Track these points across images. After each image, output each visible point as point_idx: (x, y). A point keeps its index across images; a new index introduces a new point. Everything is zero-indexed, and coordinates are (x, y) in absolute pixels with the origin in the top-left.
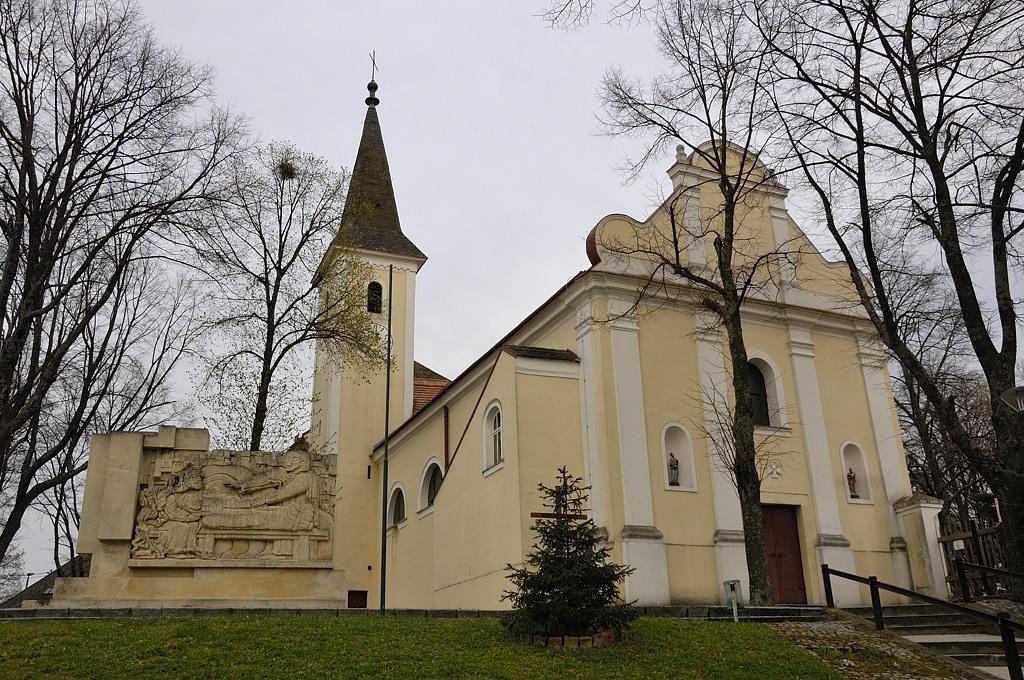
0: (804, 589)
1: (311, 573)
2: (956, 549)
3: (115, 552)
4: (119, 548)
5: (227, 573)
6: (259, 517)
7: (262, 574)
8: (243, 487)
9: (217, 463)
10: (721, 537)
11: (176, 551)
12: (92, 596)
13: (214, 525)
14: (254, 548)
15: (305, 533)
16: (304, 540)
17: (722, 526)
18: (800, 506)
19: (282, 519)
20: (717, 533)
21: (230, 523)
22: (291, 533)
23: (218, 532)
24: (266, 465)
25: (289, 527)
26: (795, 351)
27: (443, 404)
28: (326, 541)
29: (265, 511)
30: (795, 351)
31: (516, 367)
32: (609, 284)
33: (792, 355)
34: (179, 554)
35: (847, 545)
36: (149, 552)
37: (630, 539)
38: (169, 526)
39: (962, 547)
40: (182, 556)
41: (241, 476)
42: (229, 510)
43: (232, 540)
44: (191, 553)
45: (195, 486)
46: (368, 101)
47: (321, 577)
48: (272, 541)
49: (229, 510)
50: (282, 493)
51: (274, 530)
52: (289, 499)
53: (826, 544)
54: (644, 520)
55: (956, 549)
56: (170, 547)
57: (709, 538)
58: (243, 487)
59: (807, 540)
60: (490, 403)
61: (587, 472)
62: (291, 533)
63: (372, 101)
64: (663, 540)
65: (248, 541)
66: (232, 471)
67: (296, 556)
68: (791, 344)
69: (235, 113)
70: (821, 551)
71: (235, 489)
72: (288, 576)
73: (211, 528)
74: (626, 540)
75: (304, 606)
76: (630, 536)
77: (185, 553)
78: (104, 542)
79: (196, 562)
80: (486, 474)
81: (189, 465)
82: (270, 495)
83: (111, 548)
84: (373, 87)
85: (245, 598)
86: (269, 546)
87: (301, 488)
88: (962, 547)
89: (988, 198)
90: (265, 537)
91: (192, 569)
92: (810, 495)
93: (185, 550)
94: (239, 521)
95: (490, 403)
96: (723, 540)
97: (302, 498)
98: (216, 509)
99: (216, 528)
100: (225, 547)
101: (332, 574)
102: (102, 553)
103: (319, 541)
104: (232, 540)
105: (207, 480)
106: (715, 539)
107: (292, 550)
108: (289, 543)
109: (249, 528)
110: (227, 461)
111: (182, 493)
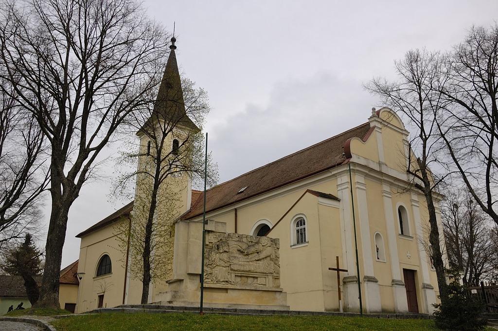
0: (418, 306)
1: (274, 293)
2: (473, 293)
3: (193, 280)
4: (195, 278)
5: (241, 292)
6: (253, 266)
7: (255, 293)
8: (246, 251)
9: (234, 240)
10: (394, 283)
11: (222, 280)
12: (186, 300)
13: (236, 269)
14: (250, 280)
15: (270, 274)
16: (271, 278)
17: (395, 278)
18: (416, 271)
19: (262, 268)
20: (393, 281)
21: (242, 269)
22: (265, 274)
23: (236, 272)
24: (252, 242)
25: (265, 272)
26: (385, 194)
27: (236, 207)
28: (278, 279)
29: (255, 263)
30: (385, 194)
31: (319, 201)
32: (357, 168)
33: (412, 205)
34: (222, 282)
35: (433, 289)
36: (210, 280)
37: (369, 282)
38: (218, 268)
39: (476, 293)
40: (224, 283)
41: (244, 247)
42: (241, 263)
43: (241, 276)
44: (227, 282)
45: (227, 250)
46: (171, 47)
47: (277, 295)
48: (257, 278)
49: (241, 263)
50: (262, 256)
51: (259, 273)
52: (263, 258)
53: (427, 288)
54: (371, 274)
55: (473, 293)
56: (219, 279)
57: (390, 283)
58: (246, 251)
59: (419, 285)
60: (296, 215)
61: (344, 251)
62: (265, 274)
63: (173, 47)
64: (379, 283)
65: (247, 277)
66: (240, 244)
67: (267, 285)
68: (412, 200)
69: (414, 50)
70: (425, 291)
71: (242, 252)
72: (265, 294)
73: (234, 270)
74: (366, 282)
75: (275, 309)
76: (368, 281)
77: (224, 282)
78: (189, 274)
79: (229, 286)
80: (293, 247)
81: (221, 240)
82: (255, 257)
83: (192, 277)
84: (173, 40)
85: (249, 304)
86: (256, 280)
87: (269, 254)
88: (476, 293)
89: (450, 144)
90: (255, 276)
91: (226, 290)
92: (420, 266)
93: (225, 280)
94: (245, 268)
95: (296, 215)
96: (396, 284)
97: (269, 258)
98: (235, 261)
99: (237, 271)
100: (239, 279)
101: (282, 294)
102: (188, 280)
103: (275, 279)
104: (241, 276)
105: (231, 247)
106: (393, 283)
107: (266, 282)
108: (264, 278)
109: (249, 271)
110: (237, 239)
111: (221, 253)
